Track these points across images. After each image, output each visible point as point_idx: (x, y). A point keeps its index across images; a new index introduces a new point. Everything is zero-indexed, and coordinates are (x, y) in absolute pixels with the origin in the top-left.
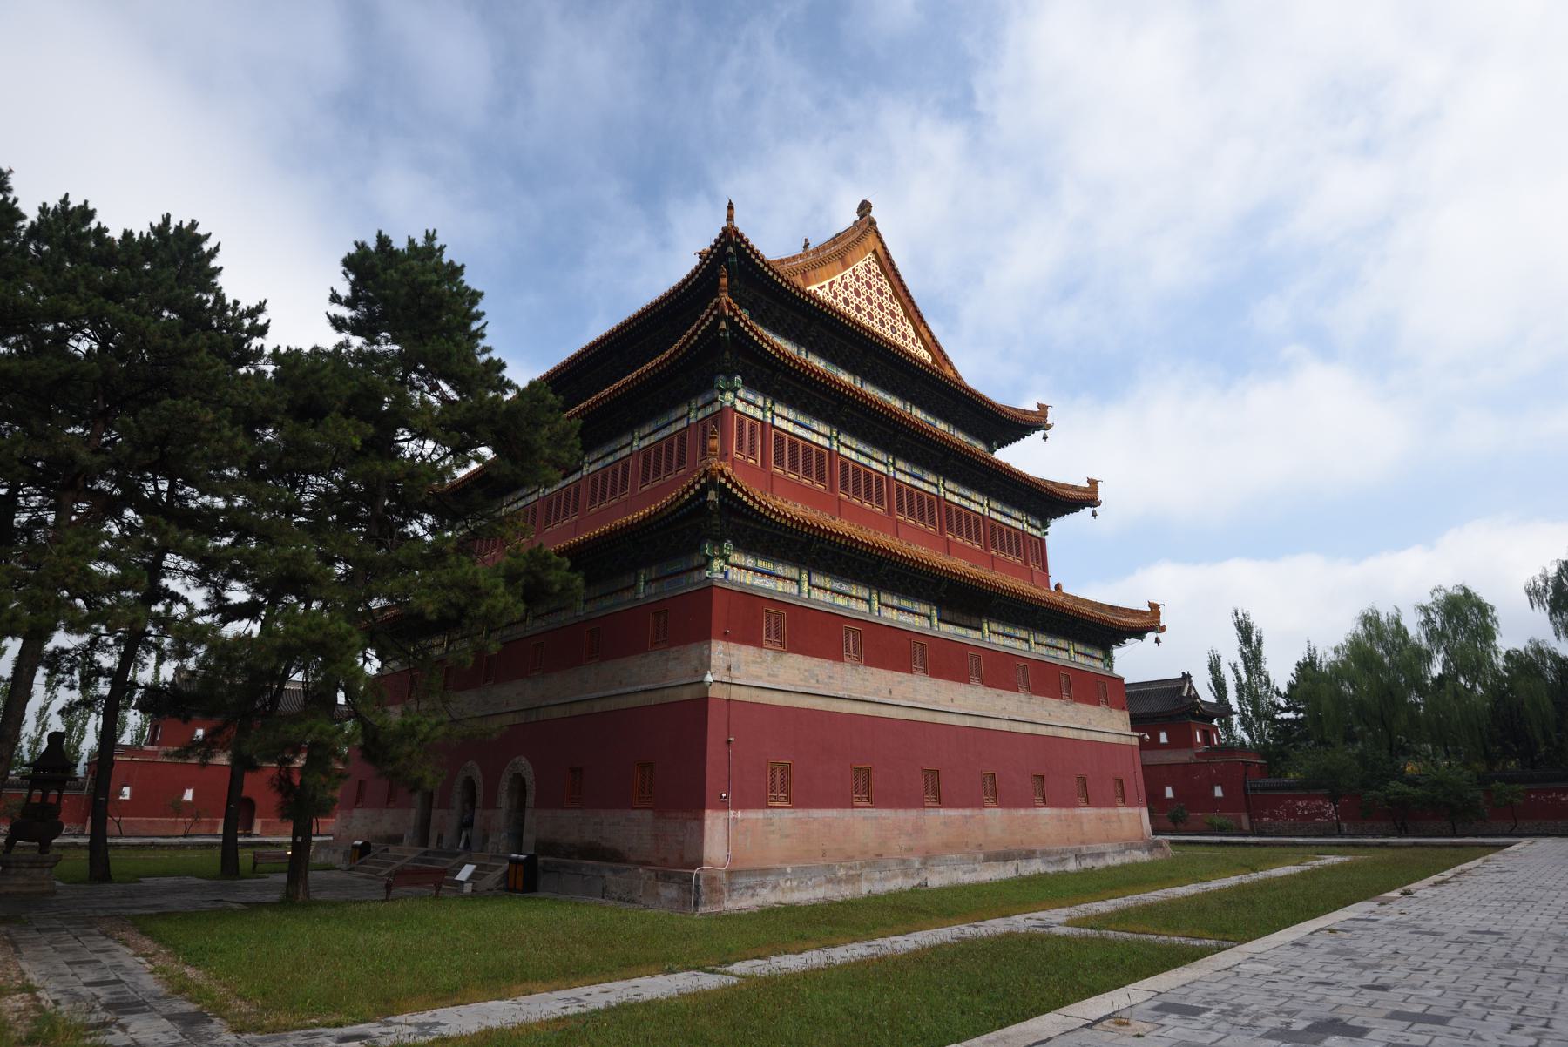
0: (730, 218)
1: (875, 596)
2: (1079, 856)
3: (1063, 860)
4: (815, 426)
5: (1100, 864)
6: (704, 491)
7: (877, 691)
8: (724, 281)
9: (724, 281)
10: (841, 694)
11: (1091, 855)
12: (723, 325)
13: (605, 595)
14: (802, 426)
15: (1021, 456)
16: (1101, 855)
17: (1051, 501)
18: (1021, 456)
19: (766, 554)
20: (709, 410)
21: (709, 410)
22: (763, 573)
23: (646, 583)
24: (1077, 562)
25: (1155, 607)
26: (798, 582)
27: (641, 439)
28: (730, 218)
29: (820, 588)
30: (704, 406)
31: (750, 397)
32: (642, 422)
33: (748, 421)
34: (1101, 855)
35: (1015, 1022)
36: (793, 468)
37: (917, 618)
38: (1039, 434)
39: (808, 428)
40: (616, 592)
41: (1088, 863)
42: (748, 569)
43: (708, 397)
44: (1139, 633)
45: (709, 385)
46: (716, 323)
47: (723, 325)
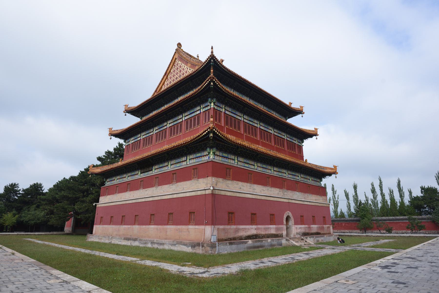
0: (212, 52)
1: (236, 158)
2: (152, 243)
3: (146, 243)
4: (237, 113)
5: (161, 247)
6: (209, 133)
7: (265, 193)
8: (212, 71)
9: (212, 71)
10: (234, 191)
11: (158, 243)
12: (212, 84)
13: (177, 163)
14: (233, 113)
15: (293, 121)
16: (163, 244)
17: (305, 135)
18: (293, 121)
19: (225, 152)
20: (206, 109)
21: (206, 109)
22: (224, 157)
23: (190, 159)
24: (313, 152)
25: (335, 167)
26: (234, 160)
27: (185, 117)
28: (212, 52)
29: (240, 162)
30: (205, 107)
31: (219, 105)
32: (185, 111)
33: (233, 119)
34: (163, 244)
35: (326, 278)
36: (235, 127)
37: (229, 160)
38: (301, 115)
39: (235, 114)
40: (181, 162)
41: (156, 246)
42: (220, 156)
43: (206, 104)
44: (330, 174)
45: (206, 101)
46: (209, 83)
47: (212, 84)
